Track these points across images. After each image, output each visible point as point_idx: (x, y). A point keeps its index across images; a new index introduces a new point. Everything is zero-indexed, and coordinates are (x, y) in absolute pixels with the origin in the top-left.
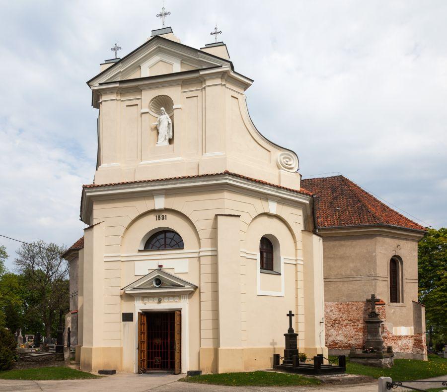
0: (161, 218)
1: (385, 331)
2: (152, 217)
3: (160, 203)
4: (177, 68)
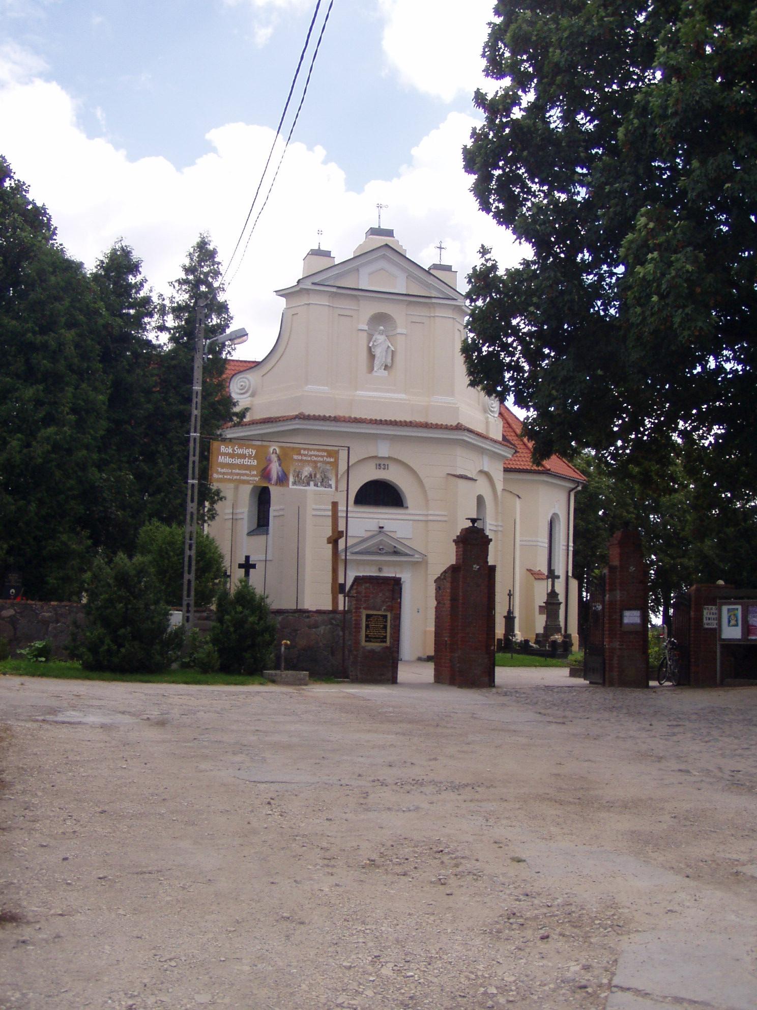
0: (382, 467)
1: (719, 862)
2: (371, 465)
3: (383, 450)
4: (401, 287)
